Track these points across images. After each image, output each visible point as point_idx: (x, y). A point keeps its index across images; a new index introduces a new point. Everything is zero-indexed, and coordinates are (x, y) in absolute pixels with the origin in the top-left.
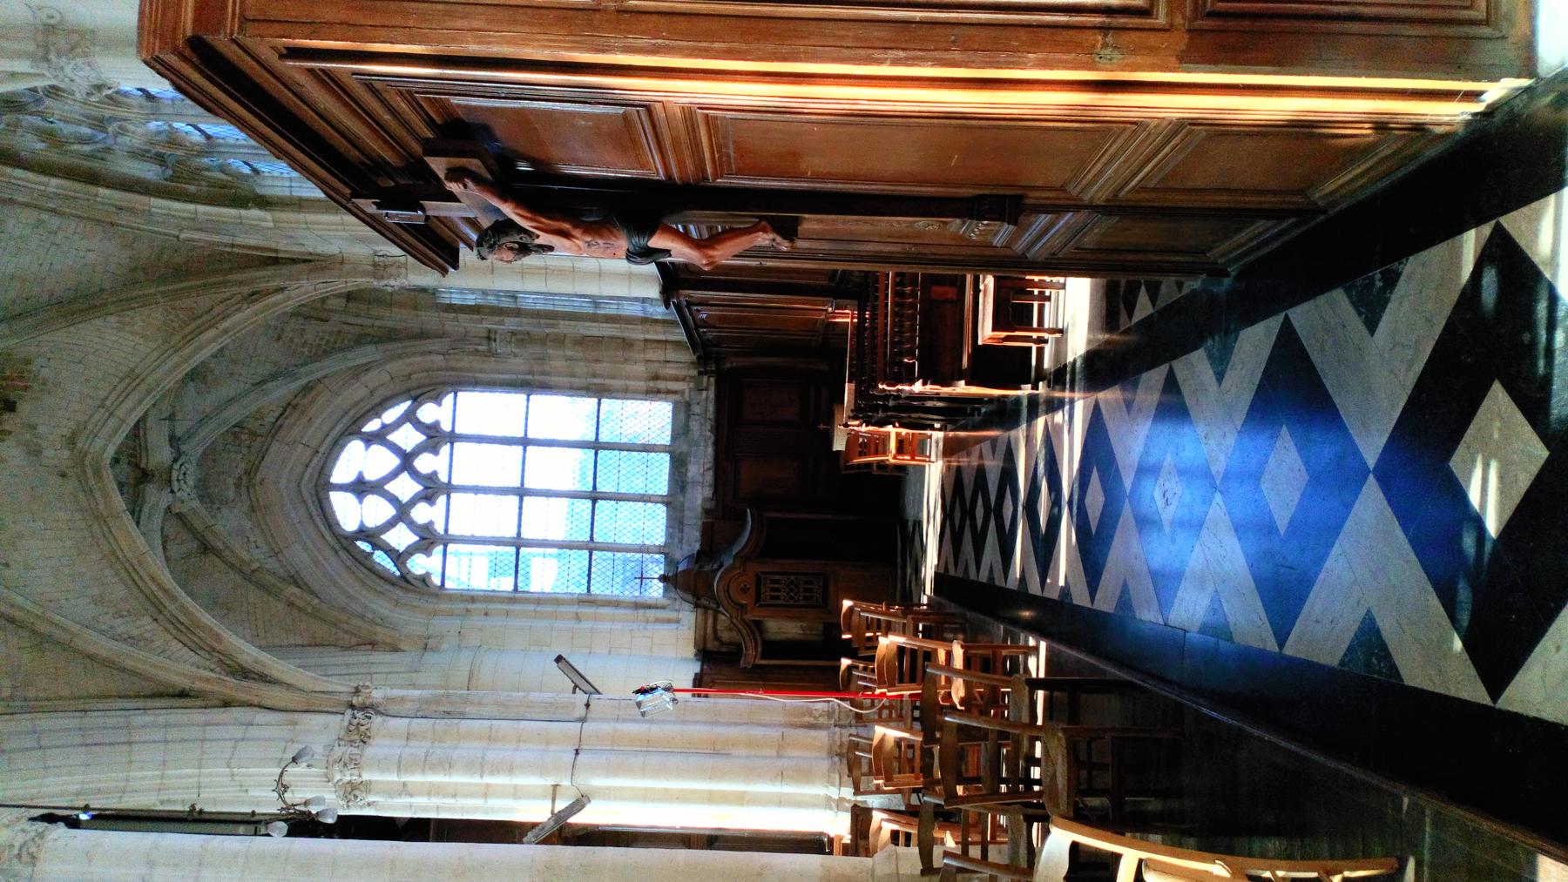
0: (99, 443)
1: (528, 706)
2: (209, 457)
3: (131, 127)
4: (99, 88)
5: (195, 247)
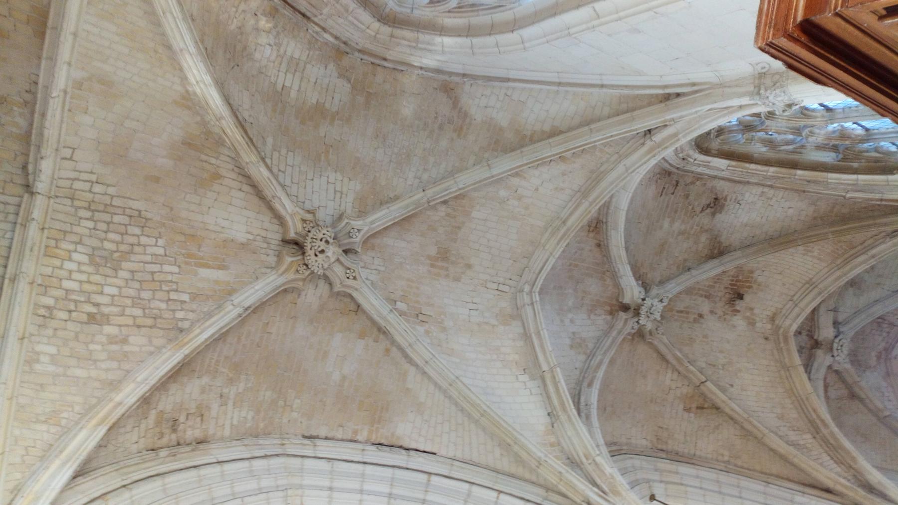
0: (788, 322)
2: (860, 336)
3: (817, 131)
4: (790, 106)
5: (855, 203)
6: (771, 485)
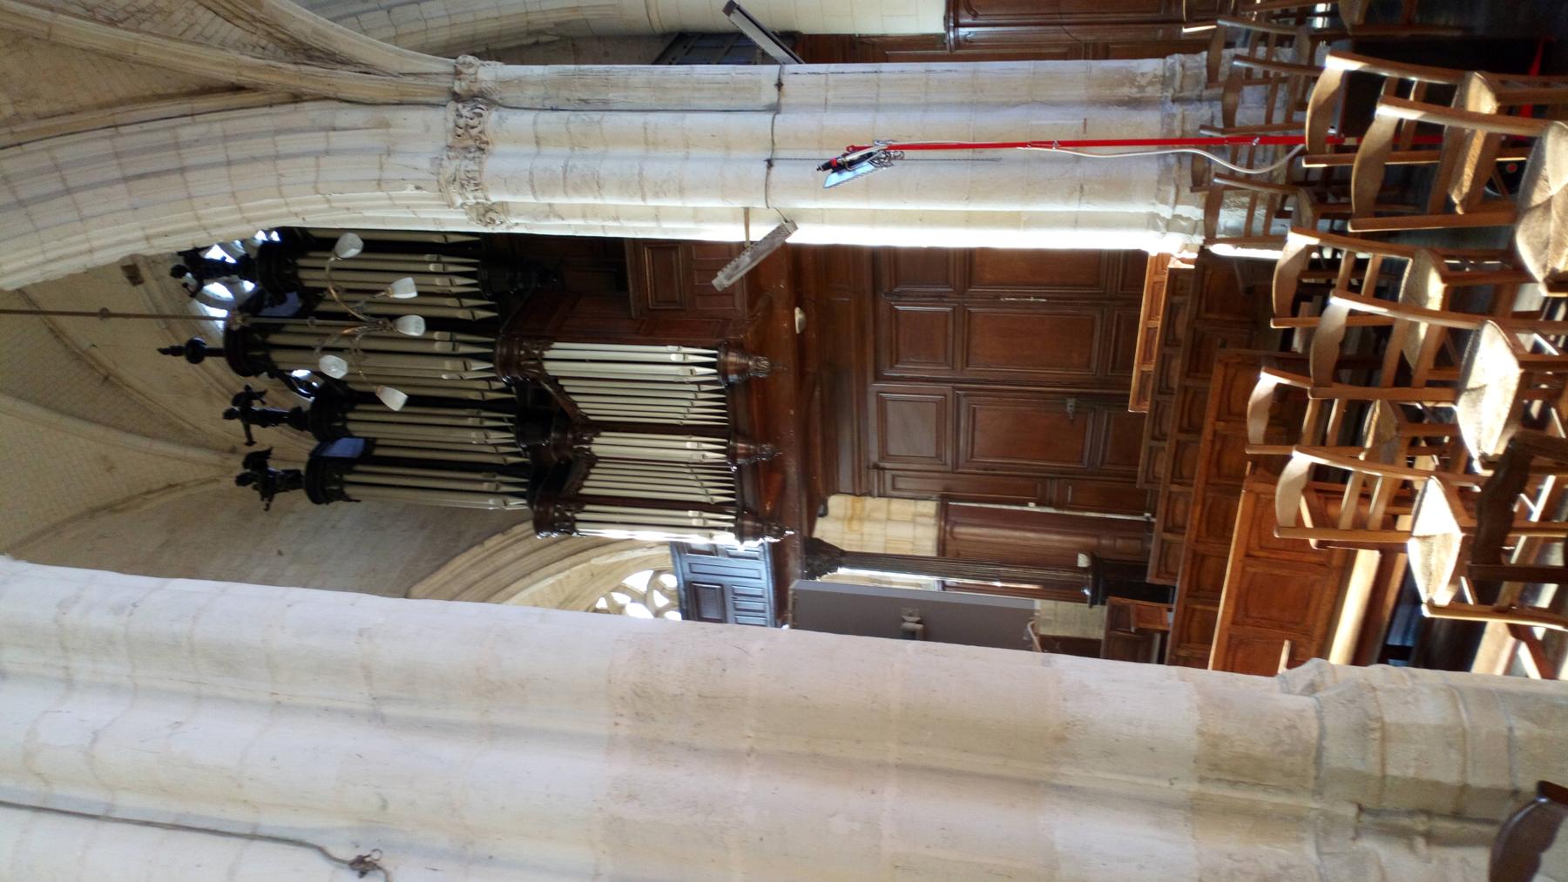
1: (695, 89)
6: (123, 130)
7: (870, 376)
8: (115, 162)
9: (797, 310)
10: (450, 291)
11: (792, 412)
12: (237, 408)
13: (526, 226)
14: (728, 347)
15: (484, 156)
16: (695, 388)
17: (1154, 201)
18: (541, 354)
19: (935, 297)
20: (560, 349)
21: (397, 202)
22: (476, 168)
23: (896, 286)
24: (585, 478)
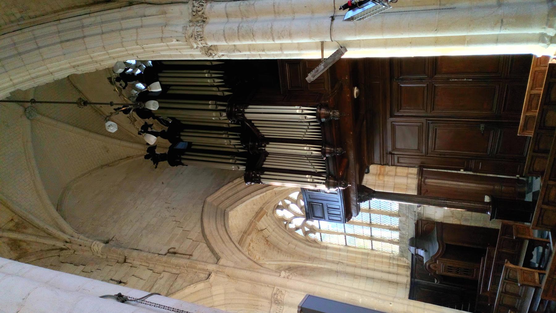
6: (61, 21)
7: (388, 116)
8: (57, 35)
9: (356, 88)
10: (214, 85)
11: (351, 133)
12: (143, 131)
13: (227, 56)
14: (321, 106)
15: (205, 24)
16: (308, 124)
17: (545, 26)
18: (244, 111)
19: (418, 80)
20: (252, 108)
21: (171, 47)
22: (201, 30)
23: (401, 76)
24: (264, 161)
